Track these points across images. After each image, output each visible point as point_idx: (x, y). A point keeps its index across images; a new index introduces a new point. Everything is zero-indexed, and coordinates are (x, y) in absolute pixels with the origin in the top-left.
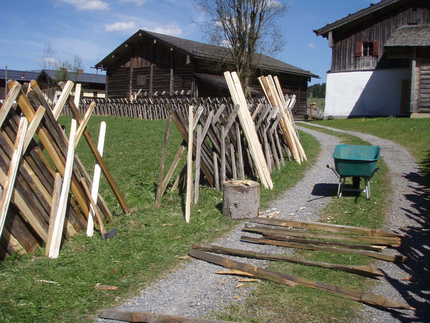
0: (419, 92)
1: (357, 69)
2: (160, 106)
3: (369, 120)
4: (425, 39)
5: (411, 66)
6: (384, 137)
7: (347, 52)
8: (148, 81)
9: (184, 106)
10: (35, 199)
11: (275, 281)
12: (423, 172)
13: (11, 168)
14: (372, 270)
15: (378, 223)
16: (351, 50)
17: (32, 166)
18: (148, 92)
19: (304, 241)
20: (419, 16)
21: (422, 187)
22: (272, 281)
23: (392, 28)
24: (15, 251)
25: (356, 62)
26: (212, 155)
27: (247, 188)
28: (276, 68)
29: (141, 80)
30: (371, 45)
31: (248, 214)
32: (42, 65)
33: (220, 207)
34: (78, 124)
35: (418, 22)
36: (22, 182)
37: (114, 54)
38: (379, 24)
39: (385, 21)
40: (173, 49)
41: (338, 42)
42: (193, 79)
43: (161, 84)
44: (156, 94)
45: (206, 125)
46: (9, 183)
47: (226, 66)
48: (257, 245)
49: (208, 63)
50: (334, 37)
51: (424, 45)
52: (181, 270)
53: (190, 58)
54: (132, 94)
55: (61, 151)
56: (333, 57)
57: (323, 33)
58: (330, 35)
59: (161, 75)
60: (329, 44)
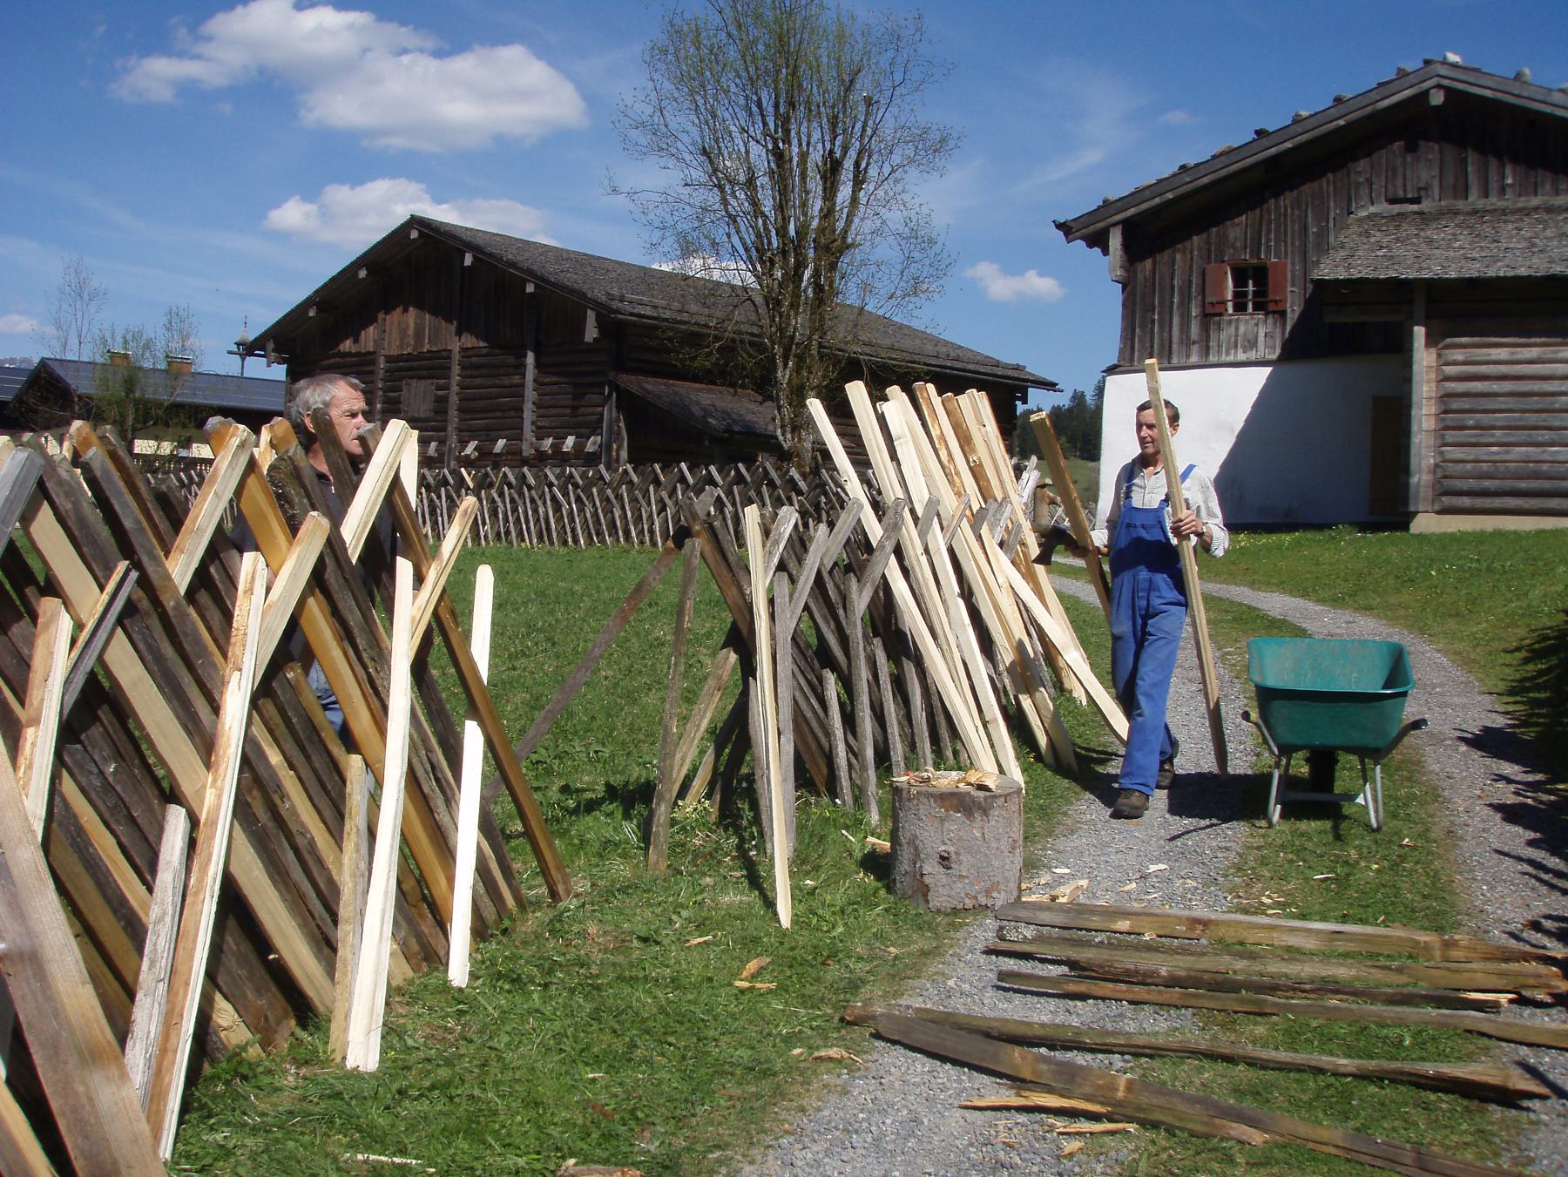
0: (1439, 442)
1: (1212, 359)
2: (501, 495)
3: (1264, 539)
4: (1451, 254)
5: (1410, 350)
6: (1336, 602)
8: (441, 404)
9: (590, 496)
10: (291, 855)
11: (1190, 1126)
12: (1524, 724)
13: (222, 742)
14: (1508, 1076)
15: (1444, 913)
16: (1190, 293)
17: (277, 733)
18: (442, 442)
19: (1222, 985)
20: (1424, 175)
21: (1539, 777)
22: (1182, 1129)
23: (1332, 215)
24: (225, 1048)
25: (1208, 336)
26: (821, 680)
27: (986, 798)
28: (916, 358)
30: (1260, 274)
31: (988, 893)
32: (55, 343)
33: (879, 865)
34: (419, 579)
35: (1423, 193)
36: (250, 791)
37: (317, 304)
38: (1287, 199)
39: (1307, 189)
40: (536, 286)
41: (1142, 259)
42: (610, 394)
44: (470, 449)
45: (805, 573)
46: (219, 797)
47: (734, 349)
48: (1062, 1003)
49: (670, 339)
50: (1126, 246)
51: (1453, 275)
52: (833, 1098)
55: (368, 674)
56: (1124, 316)
57: (1087, 230)
58: (1115, 241)
59: (490, 382)
60: (1112, 270)
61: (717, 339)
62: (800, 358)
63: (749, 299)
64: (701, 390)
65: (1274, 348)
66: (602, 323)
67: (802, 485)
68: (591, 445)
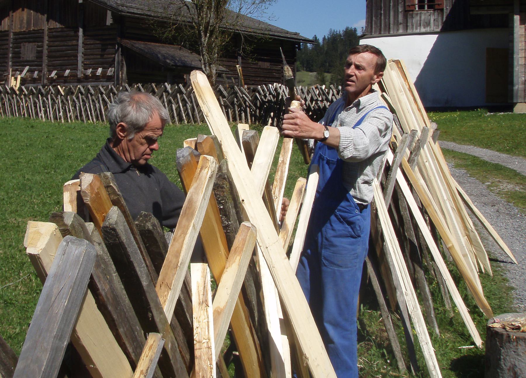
1: (409, 31)
2: (78, 98)
5: (513, 27)
7: (391, 4)
8: (39, 55)
18: (40, 71)
29: (28, 51)
42: (118, 49)
43: (63, 58)
44: (53, 74)
53: (112, 15)
54: (12, 75)
61: (174, 24)
62: (212, 33)
63: (186, 5)
64: (159, 46)
65: (438, 26)
66: (113, 15)
67: (225, 93)
68: (110, 72)
